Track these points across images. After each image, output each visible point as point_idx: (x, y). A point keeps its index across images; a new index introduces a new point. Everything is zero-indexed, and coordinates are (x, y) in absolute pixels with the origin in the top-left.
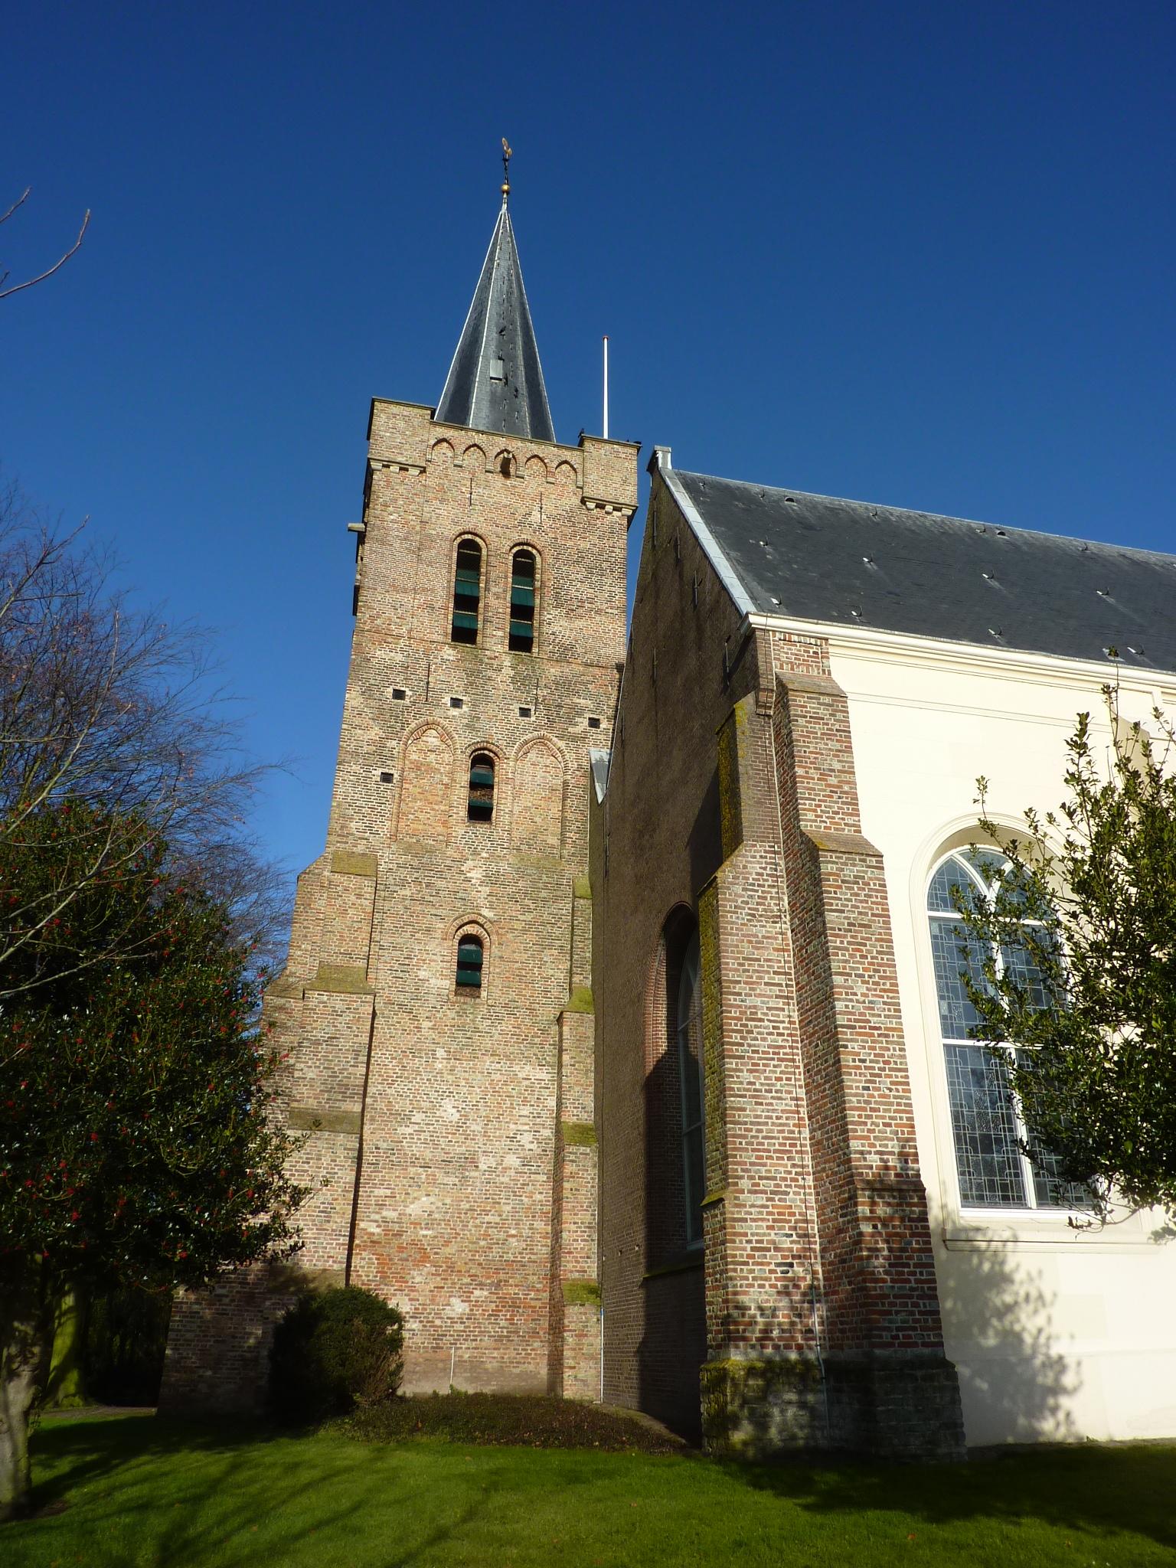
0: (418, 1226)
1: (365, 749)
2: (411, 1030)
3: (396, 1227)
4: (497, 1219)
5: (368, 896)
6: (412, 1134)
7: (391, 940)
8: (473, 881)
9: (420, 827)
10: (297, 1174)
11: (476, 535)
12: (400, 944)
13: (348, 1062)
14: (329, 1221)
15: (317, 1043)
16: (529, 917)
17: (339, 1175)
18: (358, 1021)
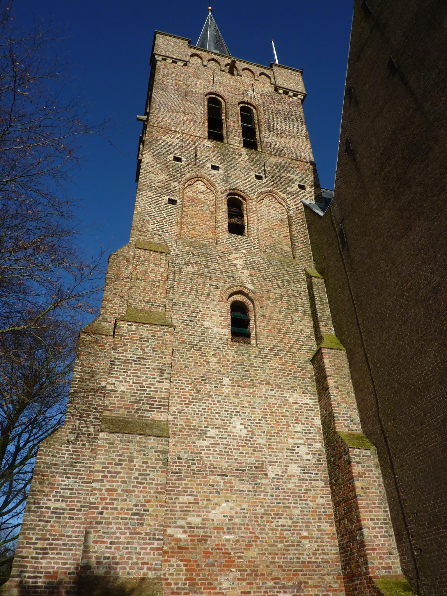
0: (221, 531)
1: (157, 185)
2: (201, 363)
3: (201, 532)
4: (289, 522)
5: (163, 266)
6: (209, 447)
7: (181, 299)
8: (238, 266)
9: (197, 233)
10: (109, 475)
11: (218, 95)
12: (188, 302)
13: (154, 378)
14: (142, 524)
15: (127, 362)
16: (279, 291)
17: (151, 476)
18: (163, 346)
